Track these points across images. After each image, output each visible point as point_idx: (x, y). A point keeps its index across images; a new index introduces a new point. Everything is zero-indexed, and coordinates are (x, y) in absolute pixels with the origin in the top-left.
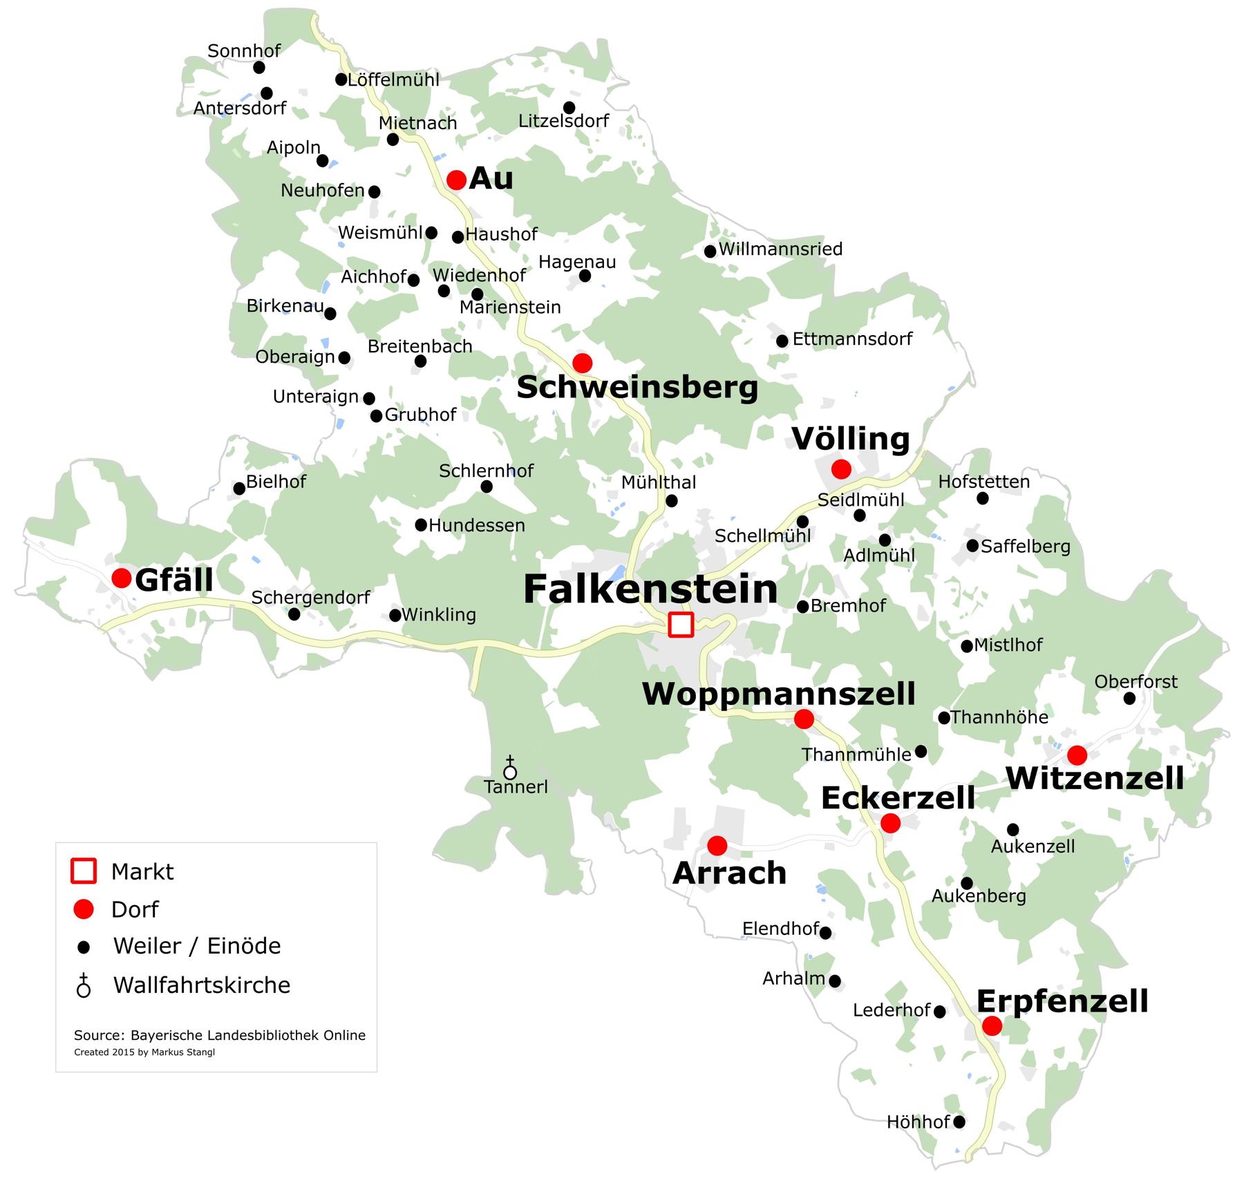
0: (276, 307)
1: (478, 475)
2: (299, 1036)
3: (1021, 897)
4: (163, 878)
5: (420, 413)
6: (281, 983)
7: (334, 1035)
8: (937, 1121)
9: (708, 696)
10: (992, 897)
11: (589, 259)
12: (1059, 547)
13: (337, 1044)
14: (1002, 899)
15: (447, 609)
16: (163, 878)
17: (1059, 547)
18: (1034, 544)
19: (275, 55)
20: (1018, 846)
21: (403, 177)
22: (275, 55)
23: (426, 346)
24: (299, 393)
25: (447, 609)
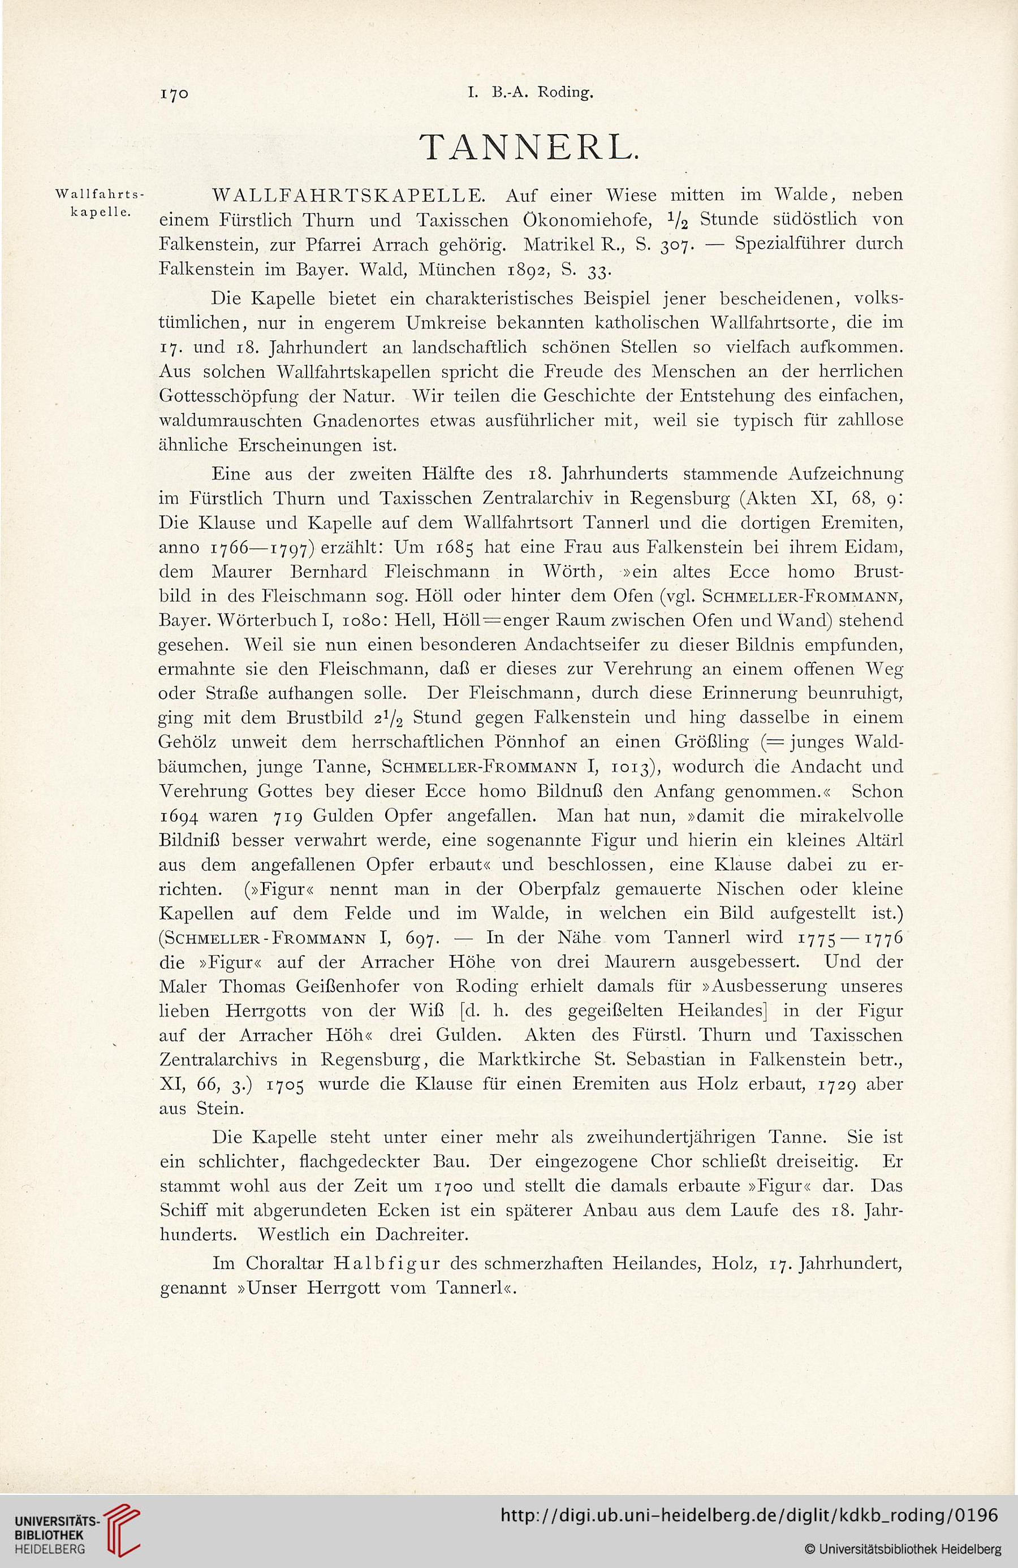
0: (865, 1516)
1: (674, 1519)
2: (921, 1549)
3: (745, 1516)
4: (847, 1520)
5: (610, 1514)
6: (810, 1522)
7: (829, 1549)
8: (901, 1514)
9: (564, 1517)
10: (718, 1517)
11: (855, 1521)
12: (738, 1516)
13: (831, 1556)
14: (727, 1518)
15: (816, 1509)
16: (847, 1520)
17: (738, 1516)
18: (715, 1514)
19: (45, 1532)
20: (864, 1515)
21: (107, 1548)
22: (45, 1532)
23: (930, 1514)
24: (514, 1512)
25: (816, 1509)
